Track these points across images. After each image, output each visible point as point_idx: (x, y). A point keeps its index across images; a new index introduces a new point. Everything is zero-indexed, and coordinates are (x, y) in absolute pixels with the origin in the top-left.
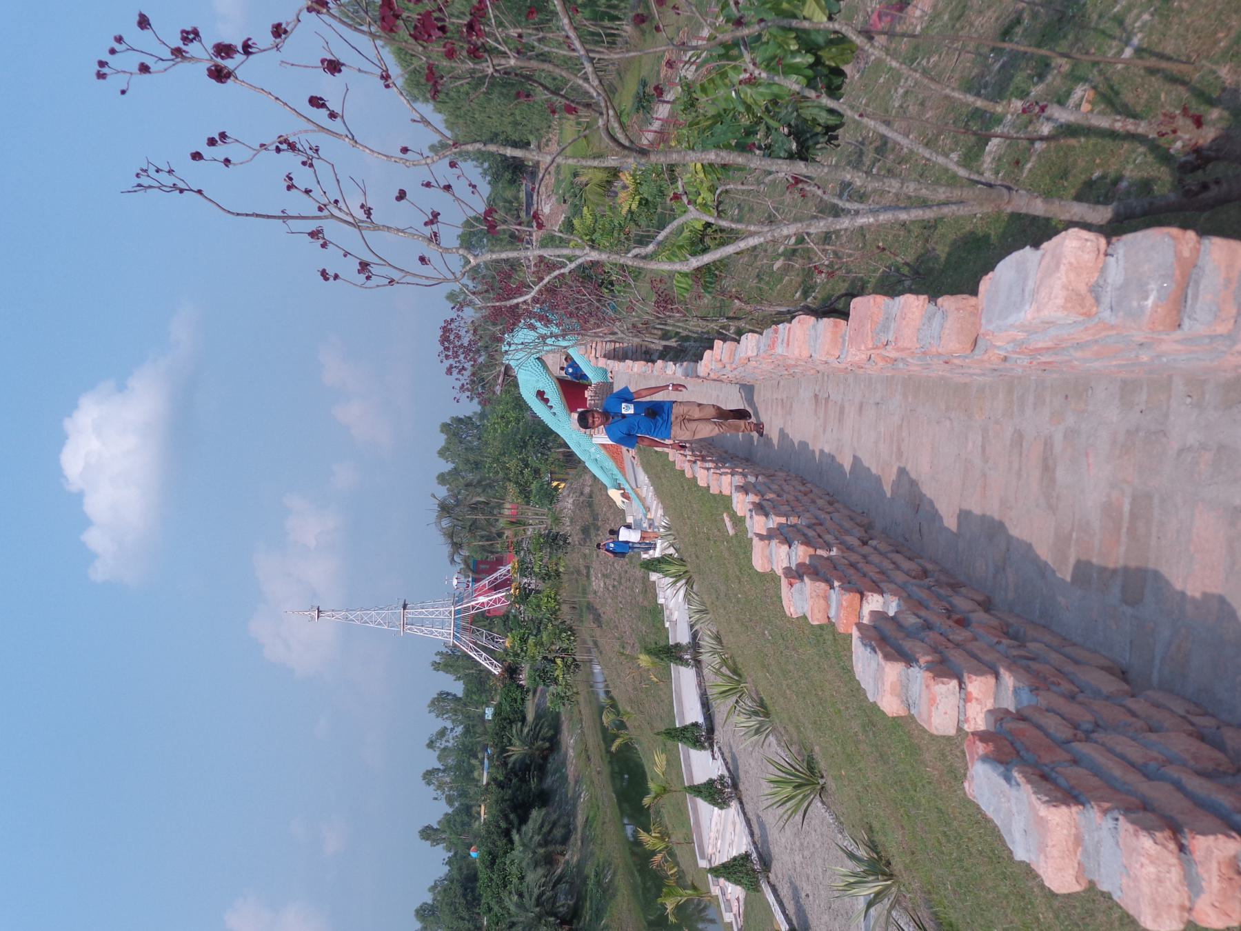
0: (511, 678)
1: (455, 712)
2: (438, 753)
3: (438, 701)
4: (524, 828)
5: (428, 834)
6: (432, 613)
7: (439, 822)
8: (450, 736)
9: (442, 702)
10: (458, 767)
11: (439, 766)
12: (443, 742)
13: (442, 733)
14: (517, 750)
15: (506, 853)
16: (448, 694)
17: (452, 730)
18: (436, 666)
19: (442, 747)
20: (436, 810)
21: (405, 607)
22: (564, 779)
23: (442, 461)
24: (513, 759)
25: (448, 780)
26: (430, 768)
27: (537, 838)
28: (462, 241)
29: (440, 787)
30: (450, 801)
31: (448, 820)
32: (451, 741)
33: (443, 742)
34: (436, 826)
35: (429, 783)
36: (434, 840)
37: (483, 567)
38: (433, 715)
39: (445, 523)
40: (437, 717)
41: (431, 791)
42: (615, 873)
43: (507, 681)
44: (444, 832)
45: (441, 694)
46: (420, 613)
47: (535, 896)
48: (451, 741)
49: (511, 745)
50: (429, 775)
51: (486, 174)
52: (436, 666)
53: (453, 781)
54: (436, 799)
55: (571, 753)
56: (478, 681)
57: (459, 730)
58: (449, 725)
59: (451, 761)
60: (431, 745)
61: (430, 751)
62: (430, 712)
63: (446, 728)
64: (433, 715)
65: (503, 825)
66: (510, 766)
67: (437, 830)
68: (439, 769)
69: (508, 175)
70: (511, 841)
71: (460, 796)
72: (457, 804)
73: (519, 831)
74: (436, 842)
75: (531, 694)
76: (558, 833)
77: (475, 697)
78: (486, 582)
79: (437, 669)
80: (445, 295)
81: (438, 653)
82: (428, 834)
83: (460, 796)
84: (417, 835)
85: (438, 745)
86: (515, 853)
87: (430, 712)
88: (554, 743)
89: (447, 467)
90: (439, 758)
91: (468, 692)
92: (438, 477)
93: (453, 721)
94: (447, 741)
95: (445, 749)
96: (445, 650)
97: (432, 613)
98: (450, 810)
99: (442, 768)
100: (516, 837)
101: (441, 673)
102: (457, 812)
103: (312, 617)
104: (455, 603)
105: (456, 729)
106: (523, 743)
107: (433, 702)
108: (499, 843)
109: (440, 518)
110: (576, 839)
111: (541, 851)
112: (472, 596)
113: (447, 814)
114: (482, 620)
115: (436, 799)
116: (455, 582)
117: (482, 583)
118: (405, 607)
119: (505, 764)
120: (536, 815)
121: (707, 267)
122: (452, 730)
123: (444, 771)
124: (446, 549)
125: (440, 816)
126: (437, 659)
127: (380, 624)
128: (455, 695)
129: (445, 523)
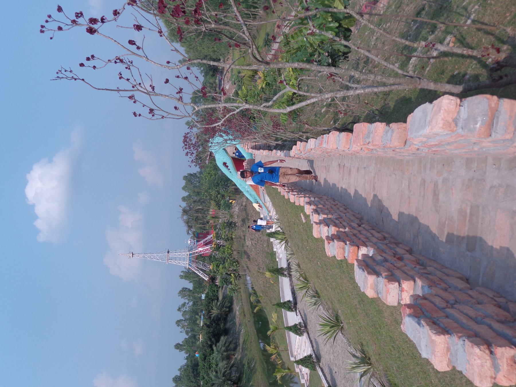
0: (213, 282)
1: (189, 296)
2: (182, 313)
3: (182, 291)
4: (218, 344)
5: (178, 346)
6: (180, 255)
7: (183, 342)
8: (187, 306)
9: (184, 292)
10: (190, 319)
11: (182, 318)
12: (184, 308)
13: (184, 305)
14: (215, 312)
15: (210, 354)
16: (186, 288)
17: (188, 303)
18: (181, 277)
19: (184, 310)
20: (181, 337)
21: (168, 252)
22: (235, 324)
23: (184, 192)
24: (213, 315)
25: (186, 324)
26: (179, 319)
27: (223, 348)
28: (192, 100)
29: (183, 327)
30: (187, 333)
31: (186, 341)
32: (188, 308)
33: (184, 308)
34: (181, 343)
35: (178, 326)
36: (180, 349)
37: (201, 235)
38: (180, 297)
39: (185, 217)
40: (182, 298)
41: (179, 329)
42: (256, 363)
43: (211, 283)
44: (185, 346)
45: (183, 288)
46: (175, 255)
47: (222, 372)
48: (188, 308)
49: (213, 310)
50: (178, 322)
51: (202, 72)
52: (181, 277)
53: (188, 325)
54: (181, 332)
55: (237, 313)
56: (199, 283)
57: (191, 303)
58: (187, 301)
59: (187, 317)
60: (179, 310)
61: (179, 312)
62: (179, 296)
63: (185, 303)
64: (180, 297)
65: (209, 343)
67: (182, 345)
68: (182, 320)
69: (211, 73)
70: (213, 350)
71: (191, 331)
72: (190, 334)
73: (216, 345)
74: (181, 350)
76: (232, 346)
77: (197, 290)
78: (202, 242)
79: (182, 278)
80: (185, 122)
81: (182, 272)
82: (178, 346)
83: (191, 331)
84: (173, 347)
85: (182, 310)
86: (214, 354)
87: (179, 296)
88: (230, 309)
89: (186, 194)
90: (183, 315)
91: (195, 288)
92: (182, 198)
93: (188, 300)
95: (185, 311)
96: (185, 270)
97: (180, 255)
98: (187, 337)
99: (184, 319)
100: (214, 348)
101: (183, 280)
102: (190, 338)
103: (130, 257)
105: (190, 303)
106: (218, 309)
107: (180, 292)
109: (183, 215)
110: (239, 349)
111: (225, 354)
112: (196, 248)
113: (186, 338)
114: (200, 258)
115: (181, 332)
116: (189, 242)
117: (200, 242)
118: (168, 252)
119: (210, 318)
121: (294, 111)
122: (188, 303)
123: (185, 321)
124: (185, 228)
125: (183, 339)
126: (182, 274)
127: (158, 259)
128: (189, 289)
129: (185, 217)
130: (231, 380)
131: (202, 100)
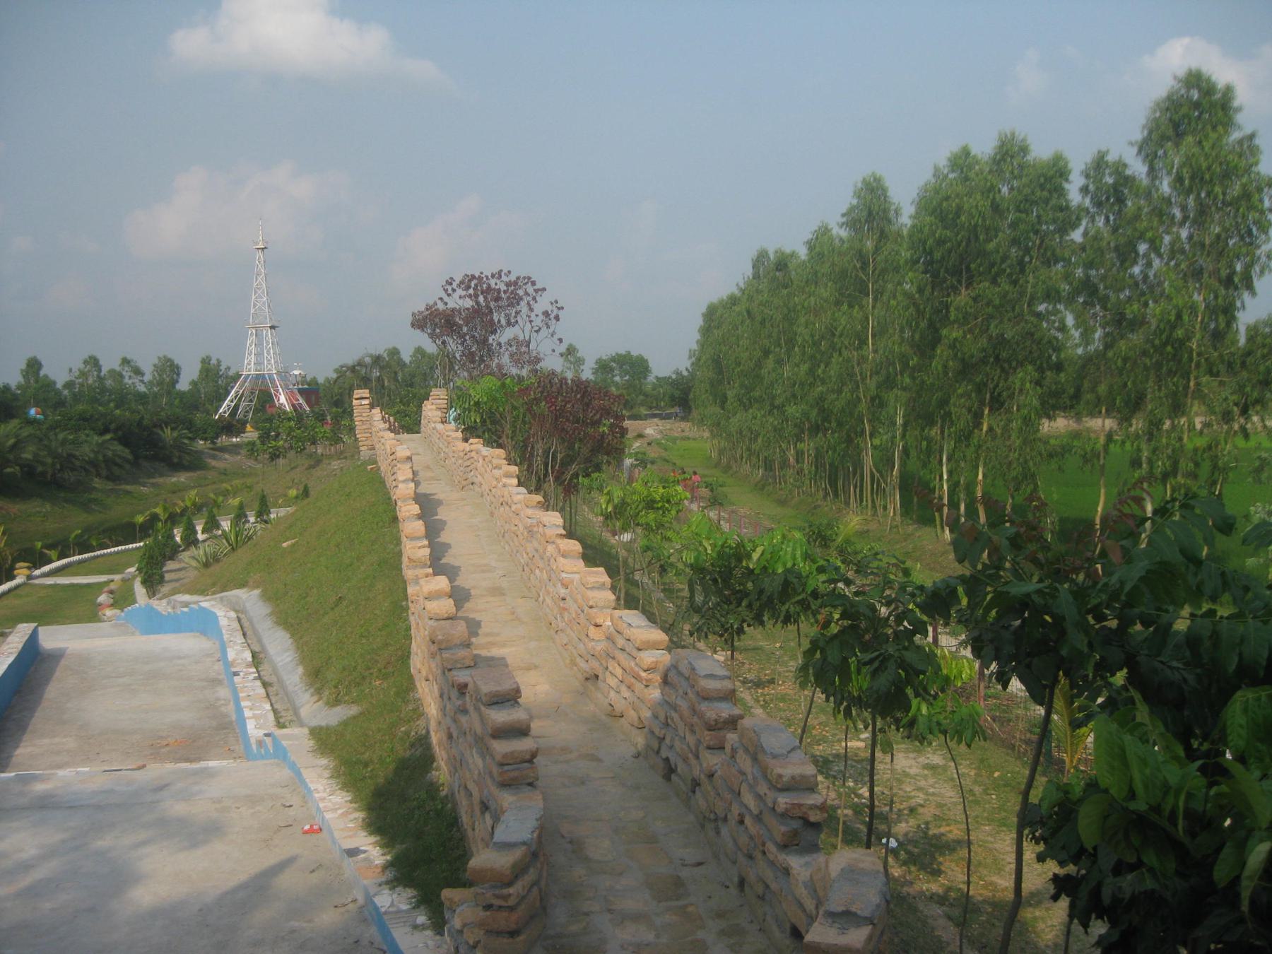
0: (223, 428)
1: (160, 383)
2: (118, 369)
3: (171, 366)
4: (115, 442)
5: (34, 366)
6: (268, 353)
7: (46, 376)
8: (136, 380)
9: (170, 369)
10: (103, 390)
11: (104, 371)
12: (129, 374)
13: (138, 372)
14: (168, 434)
15: (93, 429)
16: (178, 375)
17: (142, 381)
18: (206, 361)
19: (124, 373)
20: (59, 372)
21: (272, 327)
22: (151, 476)
23: (411, 352)
24: (161, 433)
25: (90, 381)
26: (101, 362)
27: (110, 454)
28: (625, 356)
29: (83, 374)
30: (69, 385)
31: (49, 385)
32: (130, 382)
33: (129, 374)
34: (42, 373)
35: (85, 362)
36: (27, 372)
37: (313, 398)
38: (156, 361)
39: (368, 360)
40: (155, 366)
41: (78, 365)
42: (100, 512)
43: (221, 425)
44: (37, 382)
45: (178, 367)
46: (267, 342)
47: (74, 452)
48: (130, 382)
49: (172, 429)
50: (93, 362)
51: (677, 373)
52: (206, 361)
53: (89, 387)
54: (71, 370)
55: (174, 480)
56: (921, 231)
57: (142, 388)
58: (147, 378)
59: (109, 383)
60: (125, 361)
61: (120, 362)
62: (159, 358)
63: (143, 374)
64: (156, 361)
65: (113, 426)
66: (155, 430)
67: (38, 374)
68: (100, 370)
69: (677, 393)
70: (102, 433)
71: (75, 395)
72: (66, 392)
73: (112, 439)
74: (25, 374)
75: (211, 446)
76: (116, 471)
77: (177, 401)
78: (301, 401)
79: (203, 361)
80: (574, 343)
81: (219, 361)
82: (34, 366)
83: (75, 395)
84: (31, 355)
85: (126, 369)
86: (96, 438)
87: (159, 358)
88: (177, 467)
89: (406, 357)
90: (112, 372)
91: (182, 395)
92: (395, 349)
93: (150, 382)
94: (130, 377)
95: (121, 376)
96: (223, 368)
97: (268, 353)
98: (59, 386)
99: (102, 374)
100: (108, 437)
101: (199, 366)
102: (58, 392)
103: (257, 243)
104: (279, 373)
105: (143, 385)
106: (175, 440)
107: (169, 360)
108: (100, 423)
109: (371, 356)
110: (110, 486)
111: (101, 458)
112: (286, 388)
113: (55, 383)
114: (265, 398)
115: (71, 370)
116: (296, 372)
117: (300, 398)
118: (272, 327)
119: (155, 426)
120: (126, 453)
121: (843, 831)
122: (142, 381)
123: (99, 376)
124: (350, 362)
125: (52, 377)
126: (214, 361)
127: (255, 305)
128: (177, 382)
129: (368, 360)
130: (61, 470)
131: (627, 378)
